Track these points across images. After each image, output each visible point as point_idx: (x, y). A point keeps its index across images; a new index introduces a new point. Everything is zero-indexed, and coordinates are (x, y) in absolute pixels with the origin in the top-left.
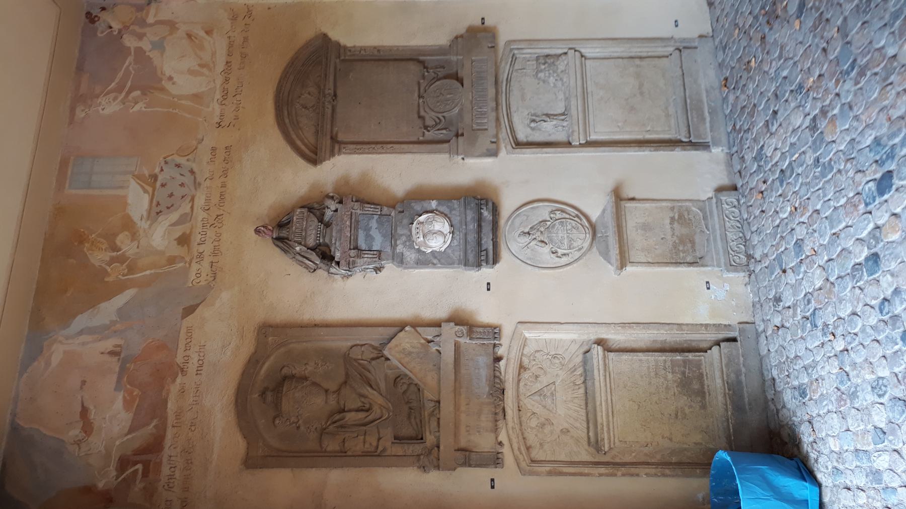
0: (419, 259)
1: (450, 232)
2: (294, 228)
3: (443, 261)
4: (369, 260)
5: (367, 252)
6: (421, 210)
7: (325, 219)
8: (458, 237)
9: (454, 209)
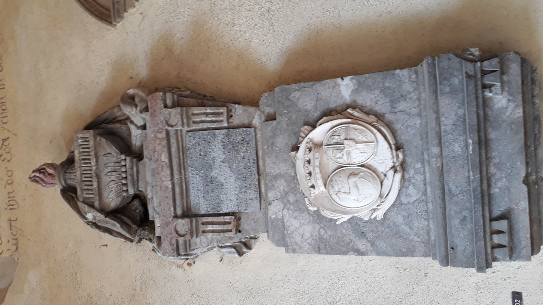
0: (321, 239)
1: (393, 167)
3: (381, 244)
6: (316, 108)
8: (419, 178)
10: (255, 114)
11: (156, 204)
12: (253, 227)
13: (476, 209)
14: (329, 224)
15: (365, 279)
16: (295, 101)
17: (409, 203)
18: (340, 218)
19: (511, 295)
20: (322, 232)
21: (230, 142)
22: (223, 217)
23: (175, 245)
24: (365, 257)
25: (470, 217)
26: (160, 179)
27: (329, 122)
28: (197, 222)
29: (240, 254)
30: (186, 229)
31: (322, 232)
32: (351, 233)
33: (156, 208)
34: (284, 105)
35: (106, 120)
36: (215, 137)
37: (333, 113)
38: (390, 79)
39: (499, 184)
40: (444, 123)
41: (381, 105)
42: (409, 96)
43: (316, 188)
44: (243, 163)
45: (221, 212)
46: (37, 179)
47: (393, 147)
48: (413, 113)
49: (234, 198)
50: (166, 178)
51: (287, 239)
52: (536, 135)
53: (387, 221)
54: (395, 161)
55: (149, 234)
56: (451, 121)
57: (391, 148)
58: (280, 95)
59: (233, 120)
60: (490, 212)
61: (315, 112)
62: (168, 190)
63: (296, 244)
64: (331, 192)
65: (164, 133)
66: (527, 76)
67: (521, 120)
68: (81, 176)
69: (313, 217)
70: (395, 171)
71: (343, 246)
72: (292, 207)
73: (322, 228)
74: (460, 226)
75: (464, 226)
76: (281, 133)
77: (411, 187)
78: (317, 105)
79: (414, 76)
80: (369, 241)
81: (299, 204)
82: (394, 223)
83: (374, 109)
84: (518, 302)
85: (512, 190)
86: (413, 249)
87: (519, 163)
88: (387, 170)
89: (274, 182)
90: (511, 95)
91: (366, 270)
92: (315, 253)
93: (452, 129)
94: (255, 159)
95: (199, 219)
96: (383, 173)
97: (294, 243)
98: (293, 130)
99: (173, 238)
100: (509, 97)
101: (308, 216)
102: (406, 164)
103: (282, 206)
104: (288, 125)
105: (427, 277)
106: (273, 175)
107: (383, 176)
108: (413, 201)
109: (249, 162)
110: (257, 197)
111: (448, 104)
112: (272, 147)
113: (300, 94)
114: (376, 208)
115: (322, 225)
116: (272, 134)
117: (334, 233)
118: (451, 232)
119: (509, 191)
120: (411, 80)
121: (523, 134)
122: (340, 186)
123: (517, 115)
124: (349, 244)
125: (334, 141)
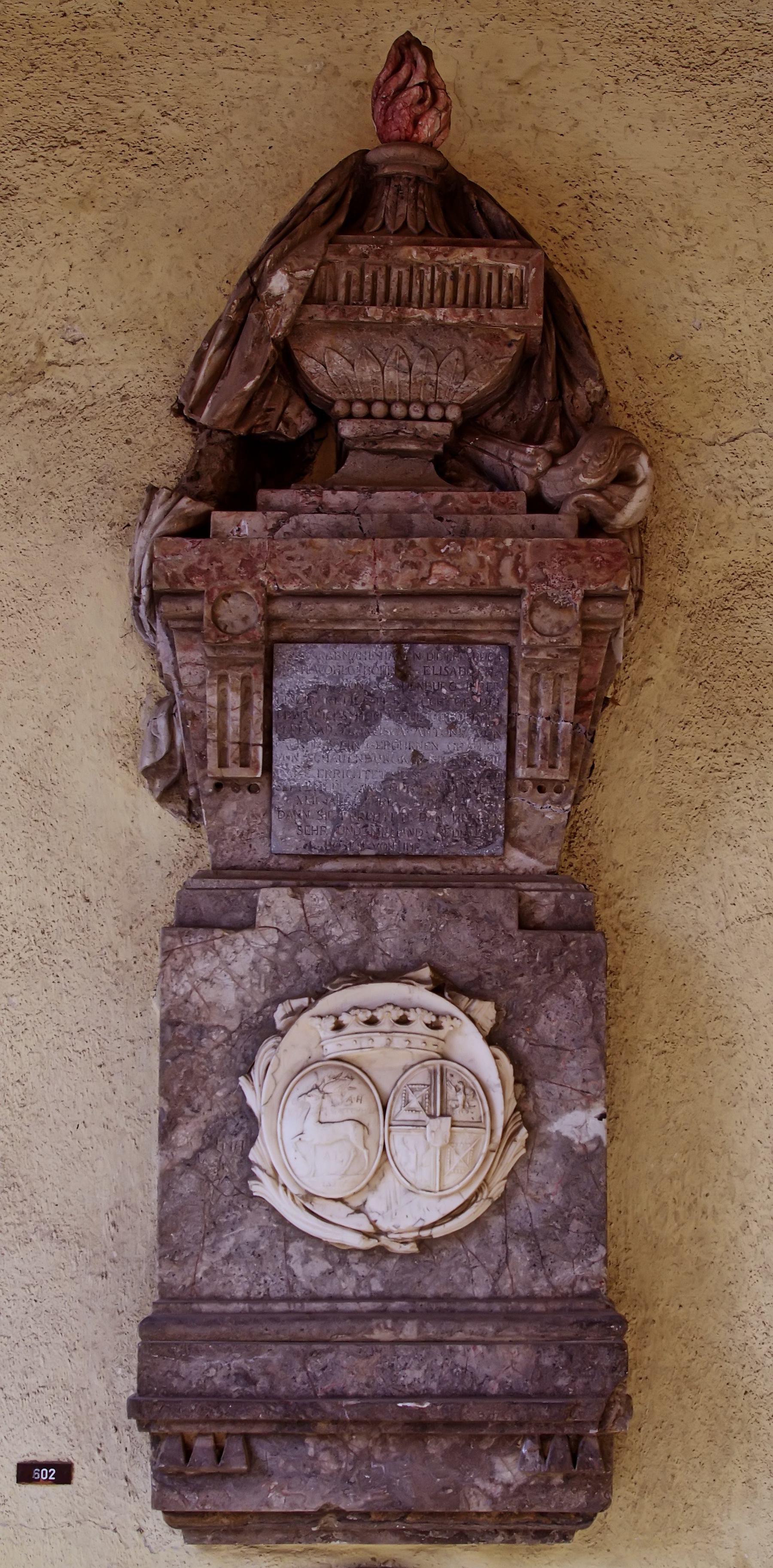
0: (202, 1030)
1: (378, 1233)
2: (414, 254)
3: (188, 1184)
4: (211, 715)
5: (258, 702)
6: (538, 1043)
7: (492, 447)
8: (348, 1286)
9: (540, 1261)
10: (539, 860)
11: (305, 521)
12: (229, 828)
13: (272, 1408)
14: (239, 1058)
15: (87, 1122)
16: (563, 986)
17: (288, 1257)
18: (254, 1089)
19: (64, 1459)
20: (218, 1036)
21: (469, 781)
22: (261, 742)
23: (188, 587)
24: (155, 1145)
25: (253, 1391)
26: (381, 555)
27: (498, 1081)
28: (251, 664)
29: (150, 773)
30: (232, 624)
31: (218, 1036)
32: (216, 1111)
33: (293, 520)
34: (556, 956)
35: (569, 346)
36: (488, 736)
37: (520, 1087)
38: (587, 1233)
39: (325, 1456)
40: (472, 1351)
41: (528, 1209)
42: (541, 1273)
43: (334, 1034)
44: (409, 813)
45: (275, 737)
46: (404, 73)
47: (425, 1234)
48: (500, 1282)
49: (312, 780)
50: (384, 573)
51: (200, 935)
52: (427, 1533)
53: (245, 1203)
54: (391, 1236)
55: (214, 474)
56: (474, 1365)
57: (422, 1229)
58: (583, 946)
59: (532, 792)
60: (259, 1436)
61: (527, 1040)
62: (349, 577)
63: (188, 960)
64: (324, 1075)
65: (515, 585)
66: (554, 1523)
67: (463, 1507)
68: (403, 263)
69: (258, 1013)
70: (367, 1235)
71: (182, 1089)
72: (283, 957)
73: (230, 1038)
74: (233, 1370)
75: (234, 1378)
76: (482, 941)
77: (326, 1266)
78: (546, 1046)
79: (585, 1288)
80: (196, 1155)
81: (292, 978)
82: (241, 1220)
83: (520, 1189)
84: (49, 1474)
85: (311, 1480)
86: (176, 1259)
87: (369, 1498)
88: (371, 1215)
89: (351, 909)
90: (520, 1490)
91: (110, 1126)
92: (164, 1010)
93: (456, 1366)
94: (417, 852)
95: (259, 669)
96: (365, 1203)
97: (188, 954)
98: (487, 977)
99: (208, 582)
100: (515, 1486)
101: (260, 999)
102: (381, 1259)
103: (289, 929)
104: (502, 962)
105: (100, 1278)
106: (372, 908)
107: (356, 1202)
108: (292, 1266)
109: (411, 833)
110: (311, 847)
111: (512, 1362)
112: (446, 911)
113: (579, 1002)
114: (278, 1182)
115: (235, 1036)
116: (482, 915)
117: (215, 1068)
118: (219, 1350)
119: (309, 1476)
120: (578, 1282)
121: (432, 1510)
122: (337, 1099)
123: (473, 1500)
124: (189, 1106)
125: (451, 1092)
